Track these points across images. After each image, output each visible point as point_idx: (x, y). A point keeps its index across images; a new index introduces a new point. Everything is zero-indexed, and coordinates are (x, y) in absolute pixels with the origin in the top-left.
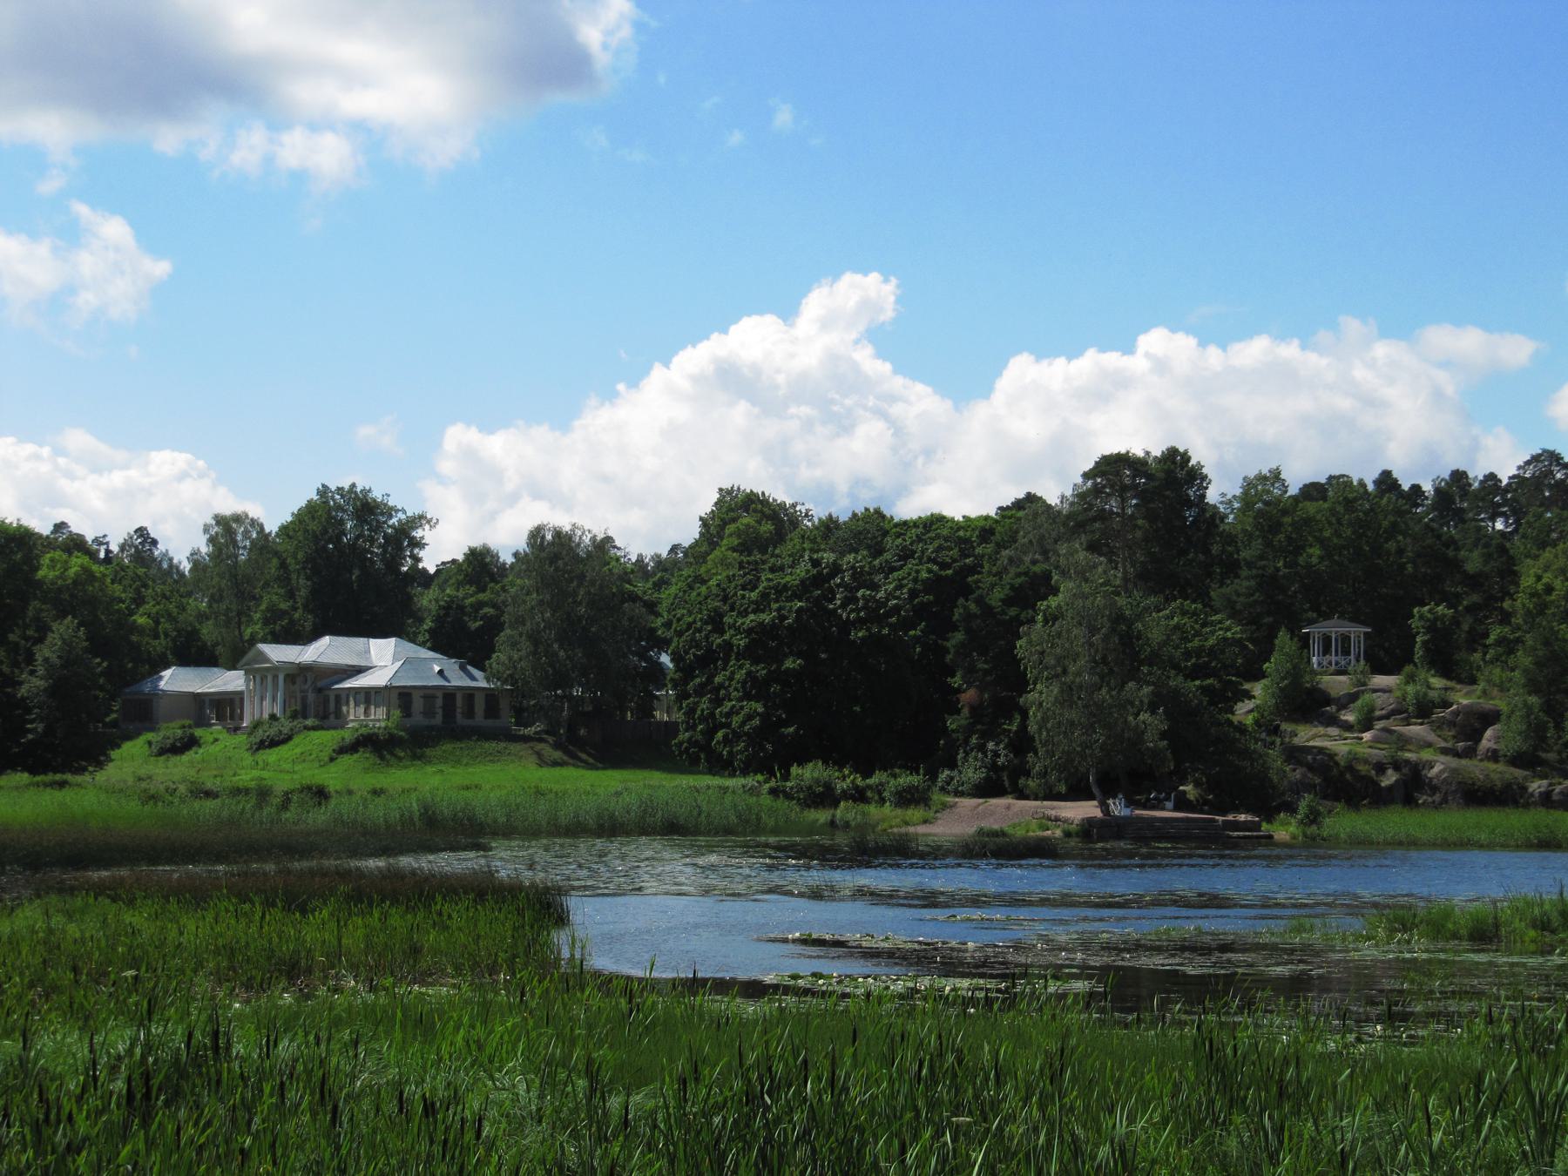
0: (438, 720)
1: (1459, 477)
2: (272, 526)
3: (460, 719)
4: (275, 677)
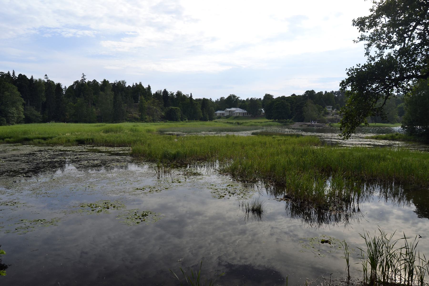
0: (243, 115)
1: (333, 91)
2: (275, 97)
3: (244, 115)
4: (228, 112)
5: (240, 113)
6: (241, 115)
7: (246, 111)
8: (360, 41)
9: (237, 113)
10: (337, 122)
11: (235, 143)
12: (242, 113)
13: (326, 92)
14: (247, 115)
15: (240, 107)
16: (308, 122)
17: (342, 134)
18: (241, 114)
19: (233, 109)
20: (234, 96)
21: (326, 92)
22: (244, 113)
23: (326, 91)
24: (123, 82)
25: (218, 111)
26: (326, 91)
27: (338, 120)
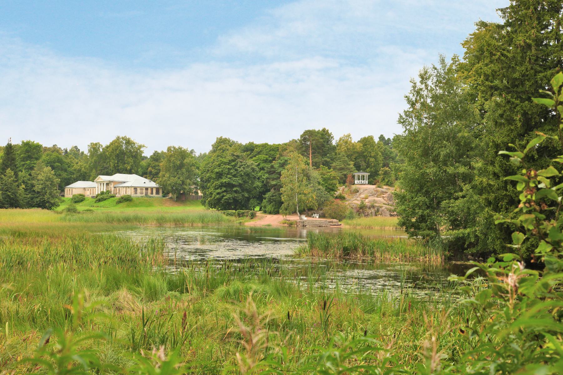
4: (104, 184)
5: (135, 189)
6: (139, 195)
7: (153, 184)
8: (368, 184)
9: (129, 187)
10: (374, 214)
11: (421, 199)
12: (141, 188)
13: (382, 138)
14: (157, 196)
15: (144, 174)
16: (290, 214)
17: (346, 295)
18: (139, 191)
19: (118, 177)
20: (128, 142)
21: (382, 138)
22: (147, 189)
23: (382, 136)
24: (76, 147)
25: (79, 182)
26: (382, 136)
27: (376, 209)
